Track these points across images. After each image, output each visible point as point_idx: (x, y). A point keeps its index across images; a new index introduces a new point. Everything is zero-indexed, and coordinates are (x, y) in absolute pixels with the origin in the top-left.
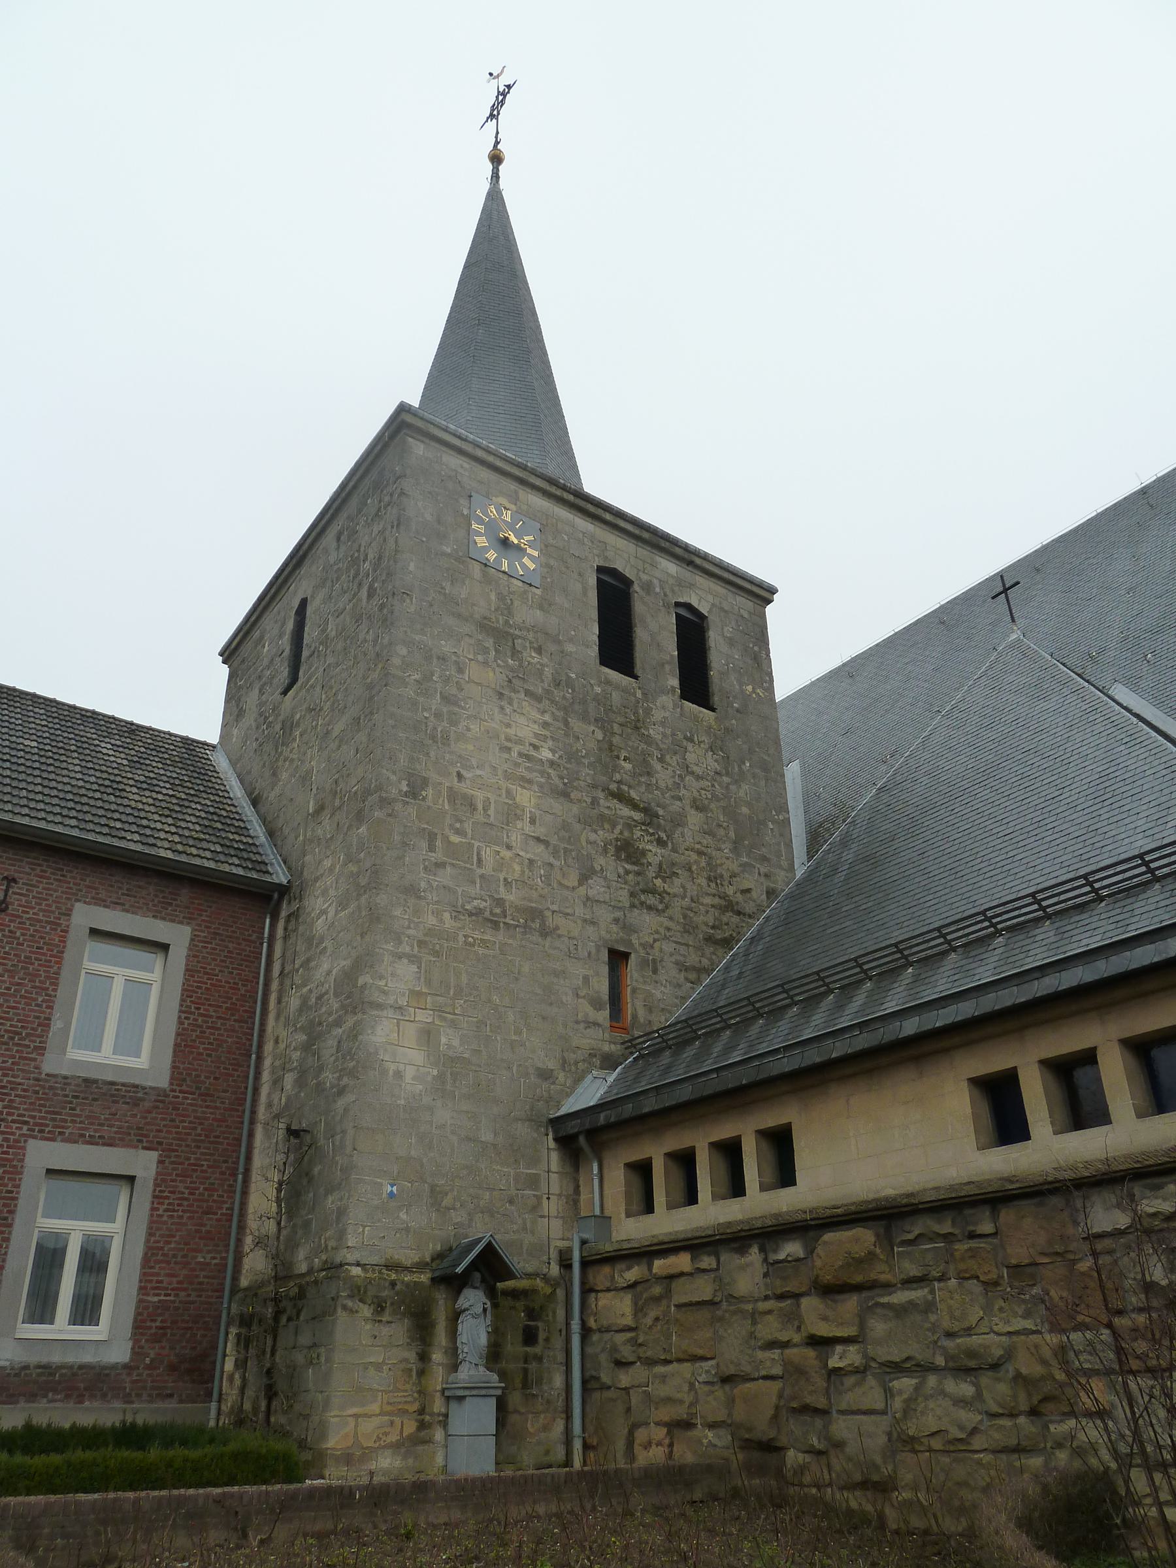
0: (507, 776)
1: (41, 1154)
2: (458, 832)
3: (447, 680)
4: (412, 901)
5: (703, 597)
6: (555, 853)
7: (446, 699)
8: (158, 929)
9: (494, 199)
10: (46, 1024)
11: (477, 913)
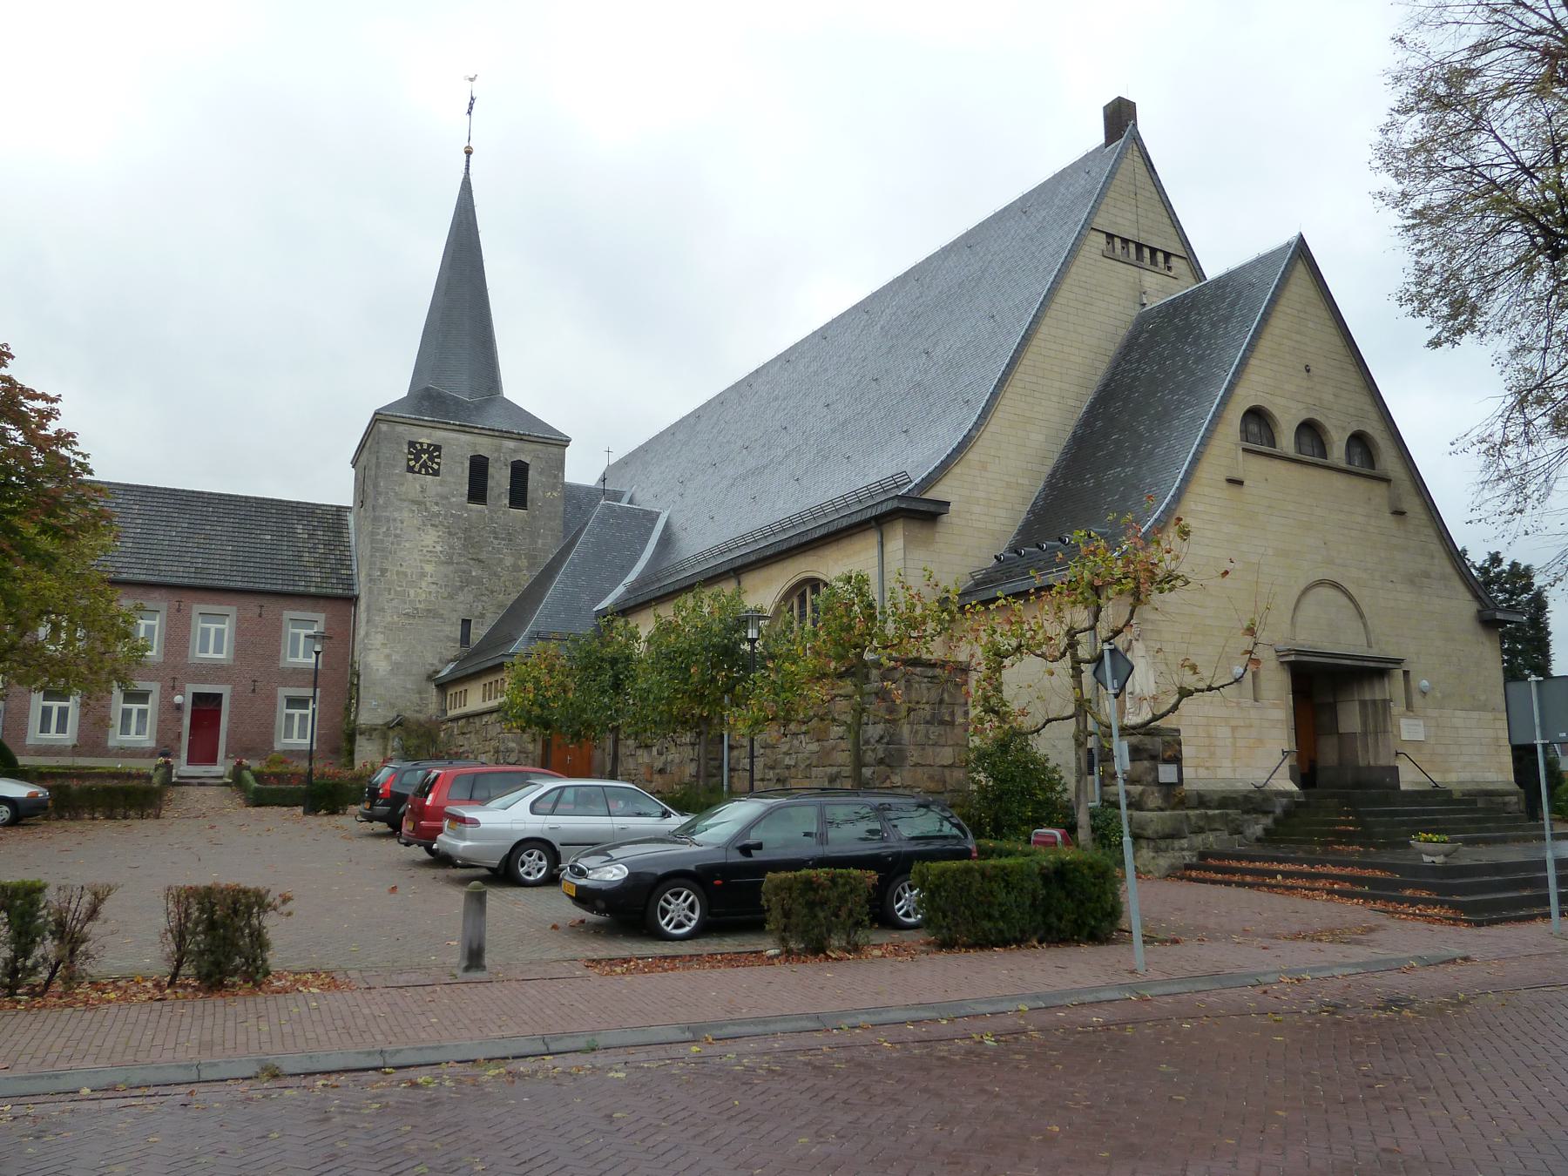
1: (283, 692)
7: (396, 536)
9: (466, 187)
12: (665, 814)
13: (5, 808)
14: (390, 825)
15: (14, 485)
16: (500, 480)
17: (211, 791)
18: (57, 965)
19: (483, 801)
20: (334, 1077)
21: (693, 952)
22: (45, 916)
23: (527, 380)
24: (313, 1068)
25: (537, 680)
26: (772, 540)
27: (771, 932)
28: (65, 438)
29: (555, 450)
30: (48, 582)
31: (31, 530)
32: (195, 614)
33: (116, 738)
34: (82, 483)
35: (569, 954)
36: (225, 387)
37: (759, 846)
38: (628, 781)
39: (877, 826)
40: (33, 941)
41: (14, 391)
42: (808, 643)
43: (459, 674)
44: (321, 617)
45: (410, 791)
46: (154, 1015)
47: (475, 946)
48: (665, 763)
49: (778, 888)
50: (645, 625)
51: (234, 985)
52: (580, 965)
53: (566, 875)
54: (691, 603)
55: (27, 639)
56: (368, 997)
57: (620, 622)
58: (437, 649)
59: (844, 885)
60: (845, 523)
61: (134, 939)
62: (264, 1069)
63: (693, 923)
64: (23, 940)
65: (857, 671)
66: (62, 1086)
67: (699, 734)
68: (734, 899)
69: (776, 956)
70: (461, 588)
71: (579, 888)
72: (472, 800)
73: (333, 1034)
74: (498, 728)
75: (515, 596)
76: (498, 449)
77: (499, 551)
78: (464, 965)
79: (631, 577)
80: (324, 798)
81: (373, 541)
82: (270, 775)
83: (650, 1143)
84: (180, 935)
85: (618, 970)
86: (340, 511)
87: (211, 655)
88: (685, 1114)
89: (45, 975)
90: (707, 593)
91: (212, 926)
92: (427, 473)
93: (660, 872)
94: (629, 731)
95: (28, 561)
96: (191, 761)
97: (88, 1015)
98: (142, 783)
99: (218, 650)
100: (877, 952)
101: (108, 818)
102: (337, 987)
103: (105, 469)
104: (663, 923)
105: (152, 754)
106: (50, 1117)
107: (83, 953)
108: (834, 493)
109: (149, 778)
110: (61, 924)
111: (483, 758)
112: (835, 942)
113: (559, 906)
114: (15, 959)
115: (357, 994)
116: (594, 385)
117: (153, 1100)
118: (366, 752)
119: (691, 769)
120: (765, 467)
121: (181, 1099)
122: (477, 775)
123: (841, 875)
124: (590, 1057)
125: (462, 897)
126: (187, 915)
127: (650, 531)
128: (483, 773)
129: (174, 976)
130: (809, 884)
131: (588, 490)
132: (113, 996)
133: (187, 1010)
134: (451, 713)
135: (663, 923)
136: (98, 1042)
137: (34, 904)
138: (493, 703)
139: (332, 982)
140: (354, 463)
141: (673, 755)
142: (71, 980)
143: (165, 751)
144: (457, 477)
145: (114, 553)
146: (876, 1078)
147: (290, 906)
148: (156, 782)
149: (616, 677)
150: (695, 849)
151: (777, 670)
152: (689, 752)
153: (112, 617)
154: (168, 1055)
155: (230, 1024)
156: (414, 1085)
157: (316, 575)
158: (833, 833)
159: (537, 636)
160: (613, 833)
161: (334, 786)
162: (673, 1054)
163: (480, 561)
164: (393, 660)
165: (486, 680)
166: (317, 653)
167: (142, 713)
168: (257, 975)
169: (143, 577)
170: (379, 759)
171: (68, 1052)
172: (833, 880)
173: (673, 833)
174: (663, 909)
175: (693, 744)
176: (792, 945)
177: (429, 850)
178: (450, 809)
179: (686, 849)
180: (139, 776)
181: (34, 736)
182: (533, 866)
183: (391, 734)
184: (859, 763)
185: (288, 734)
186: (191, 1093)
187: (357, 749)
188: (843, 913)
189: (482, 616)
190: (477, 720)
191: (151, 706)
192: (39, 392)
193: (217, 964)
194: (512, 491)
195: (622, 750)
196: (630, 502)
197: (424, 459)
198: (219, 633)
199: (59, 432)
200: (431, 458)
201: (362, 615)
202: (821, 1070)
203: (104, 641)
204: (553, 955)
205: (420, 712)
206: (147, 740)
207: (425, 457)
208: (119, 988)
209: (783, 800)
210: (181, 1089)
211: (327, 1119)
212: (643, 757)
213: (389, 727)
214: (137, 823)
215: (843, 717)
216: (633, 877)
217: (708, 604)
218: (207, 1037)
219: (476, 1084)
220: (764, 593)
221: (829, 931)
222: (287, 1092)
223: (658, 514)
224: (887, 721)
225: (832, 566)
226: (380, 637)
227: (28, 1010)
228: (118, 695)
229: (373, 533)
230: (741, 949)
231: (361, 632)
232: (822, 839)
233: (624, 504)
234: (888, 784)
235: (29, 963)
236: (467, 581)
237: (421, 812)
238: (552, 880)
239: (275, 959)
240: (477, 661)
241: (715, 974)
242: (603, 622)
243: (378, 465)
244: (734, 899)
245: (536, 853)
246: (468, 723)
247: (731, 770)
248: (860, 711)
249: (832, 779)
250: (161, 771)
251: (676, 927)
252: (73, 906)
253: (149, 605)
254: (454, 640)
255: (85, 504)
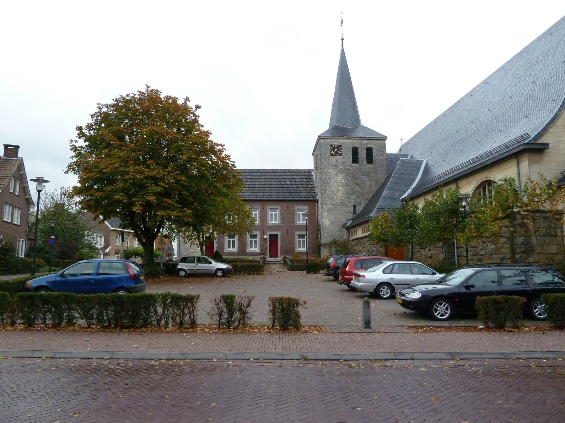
8: (304, 207)
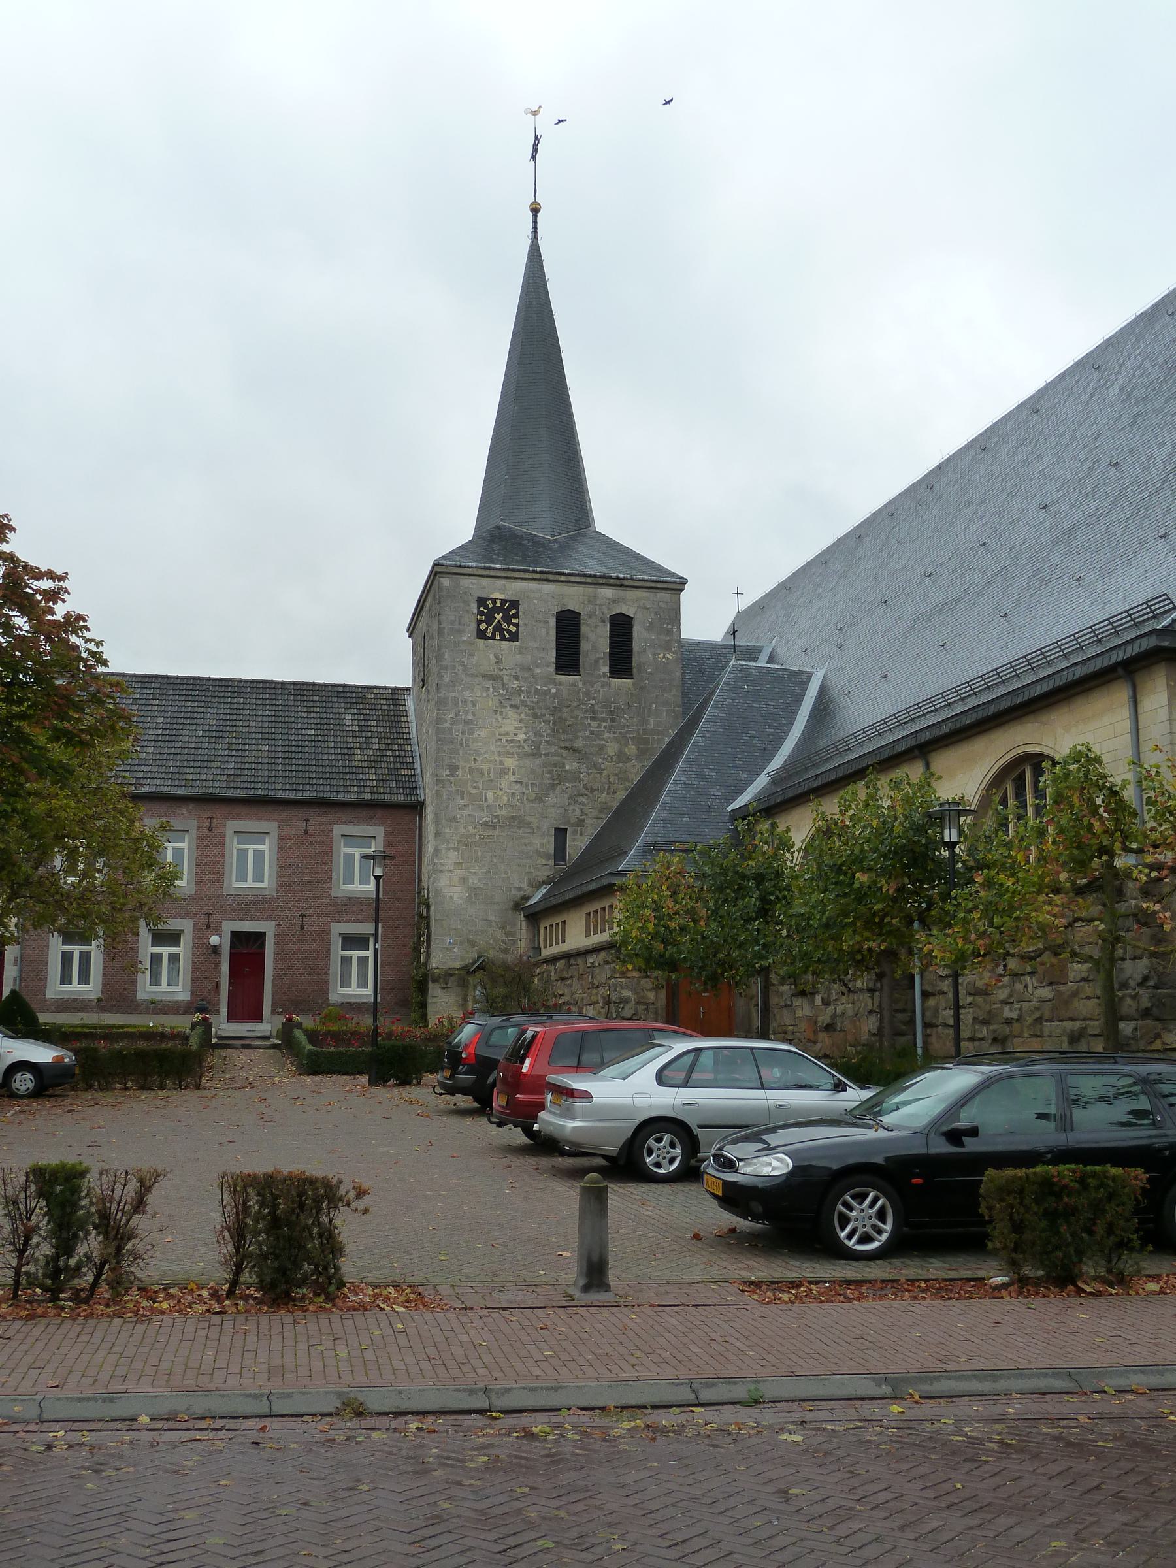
0: (500, 754)
1: (338, 929)
2: (475, 788)
3: (467, 713)
4: (453, 824)
5: (630, 604)
6: (526, 787)
7: (467, 722)
8: (370, 830)
10: (330, 878)
11: (485, 824)
12: (839, 1087)
13: (29, 1076)
14: (476, 1100)
15: (23, 685)
16: (596, 640)
17: (257, 1055)
18: (103, 1265)
19: (594, 1069)
20: (430, 1419)
21: (885, 1275)
22: (86, 1206)
23: (621, 506)
24: (405, 1405)
25: (657, 908)
26: (972, 702)
27: (995, 1253)
28: (74, 623)
29: (667, 596)
30: (65, 803)
31: (40, 736)
32: (229, 833)
33: (146, 990)
34: (96, 677)
35: (717, 1273)
36: (258, 549)
37: (973, 1132)
38: (790, 1042)
39: (1144, 1104)
40: (76, 1236)
41: (18, 572)
42: (1034, 845)
43: (554, 901)
44: (379, 831)
45: (501, 1055)
46: (214, 1332)
47: (595, 1258)
48: (834, 1017)
49: (1004, 1191)
50: (800, 828)
51: (303, 1299)
52: (734, 1288)
53: (709, 1168)
54: (862, 794)
55: (41, 871)
56: (464, 1319)
57: (764, 826)
58: (526, 869)
59: (1097, 1189)
60: (1079, 673)
61: (185, 1238)
62: (347, 1405)
63: (885, 1237)
64: (65, 1235)
65: (1108, 886)
66: (118, 1410)
67: (880, 976)
68: (943, 1205)
69: (1004, 1286)
70: (553, 787)
71: (727, 1184)
72: (580, 1067)
73: (425, 1365)
74: (608, 970)
75: (622, 795)
76: (592, 600)
77: (599, 736)
78: (582, 1282)
79: (777, 763)
80: (390, 1059)
81: (438, 731)
82: (327, 1034)
83: (842, 1530)
84: (238, 1233)
85: (785, 1296)
86: (396, 693)
87: (250, 883)
88: (887, 1496)
89: (90, 1277)
90: (884, 782)
91: (275, 1223)
92: (503, 638)
93: (835, 1166)
94: (783, 971)
95: (41, 775)
96: (232, 1017)
97: (140, 1328)
98: (178, 1046)
99: (258, 877)
100: (1152, 1286)
101: (142, 1088)
102: (425, 1305)
103: (122, 659)
104: (843, 1235)
105: (187, 1008)
106: (108, 1447)
107: (130, 1252)
108: (1060, 632)
109: (186, 1039)
110: (104, 1215)
111: (590, 1011)
112: (1088, 1269)
113: (700, 1209)
114: (56, 1258)
115: (451, 1315)
116: (714, 509)
117: (221, 1434)
118: (442, 1004)
119: (870, 1024)
120: (957, 601)
121: (253, 1435)
122: (586, 1033)
123: (1094, 1175)
124: (753, 1411)
125: (578, 1191)
126: (246, 1208)
127: (799, 699)
128: (593, 1031)
129: (234, 1283)
130: (1048, 1187)
131: (712, 647)
132: (165, 1305)
133: (251, 1327)
134: (547, 952)
135: (843, 1235)
136: (153, 1361)
137: (75, 1190)
138: (602, 938)
139: (417, 1298)
140: (412, 630)
141: (844, 1006)
142: (119, 1284)
143: (202, 1005)
144: (541, 639)
145: (136, 763)
146: (1162, 1465)
147: (366, 1201)
148: (194, 1043)
149: (763, 899)
150: (882, 1134)
151: (989, 884)
152: (866, 1002)
153: (135, 841)
154: (233, 1381)
155: (302, 1346)
156: (529, 1435)
157: (371, 778)
158: (1078, 1115)
159: (653, 848)
160: (768, 1111)
161: (405, 1048)
162: (866, 1414)
163: (575, 750)
164: (470, 886)
165: (590, 908)
166: (377, 878)
167: (174, 958)
168: (329, 1286)
169: (167, 790)
170: (458, 1014)
171: (121, 1371)
172: (1082, 1181)
173: (851, 1112)
174: (841, 1214)
175: (871, 991)
176: (1027, 1271)
177: (528, 1132)
178: (554, 1078)
179: (870, 1134)
180: (174, 1036)
181: (55, 989)
182: (664, 1155)
183: (472, 980)
184: (1113, 1014)
185: (346, 983)
186: (263, 1429)
187: (430, 1000)
188: (1100, 1229)
189: (581, 823)
190: (580, 961)
191: (183, 950)
192: (43, 569)
193: (282, 1271)
194: (612, 655)
195: (774, 1000)
196: (771, 660)
197: (499, 620)
198: (259, 855)
199: (67, 616)
200: (507, 618)
201: (430, 827)
202: (1078, 1448)
203: (126, 870)
204: (697, 1273)
205: (505, 951)
206: (177, 990)
207: (499, 617)
208: (172, 1296)
209: (1005, 1068)
210: (251, 1423)
211: (426, 1472)
212: (803, 1009)
213: (468, 971)
214: (175, 1095)
215: (1087, 950)
216: (798, 1170)
217: (886, 794)
218: (277, 1362)
219: (607, 1439)
220: (963, 778)
221: (1080, 1253)
222: (375, 1435)
223: (810, 676)
224: (1153, 955)
225: (1058, 736)
226: (453, 855)
227: (73, 1319)
228: (145, 936)
229: (438, 721)
230: (953, 1275)
231: (429, 849)
232: (1065, 1122)
233: (762, 663)
234: (1157, 1045)
235: (72, 1262)
236: (559, 778)
237: (516, 1083)
238: (690, 1173)
239: (349, 1267)
240: (578, 883)
241: (919, 1308)
242: (741, 825)
243: (440, 631)
244: (943, 1205)
245: (667, 1138)
246: (569, 965)
247: (927, 1025)
248: (1112, 941)
249: (1074, 1038)
250: (199, 1029)
251: (861, 1241)
252: (117, 1195)
253: (176, 824)
254: (547, 856)
255: (101, 703)
